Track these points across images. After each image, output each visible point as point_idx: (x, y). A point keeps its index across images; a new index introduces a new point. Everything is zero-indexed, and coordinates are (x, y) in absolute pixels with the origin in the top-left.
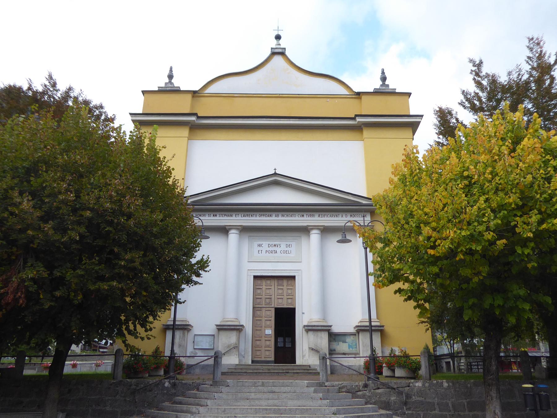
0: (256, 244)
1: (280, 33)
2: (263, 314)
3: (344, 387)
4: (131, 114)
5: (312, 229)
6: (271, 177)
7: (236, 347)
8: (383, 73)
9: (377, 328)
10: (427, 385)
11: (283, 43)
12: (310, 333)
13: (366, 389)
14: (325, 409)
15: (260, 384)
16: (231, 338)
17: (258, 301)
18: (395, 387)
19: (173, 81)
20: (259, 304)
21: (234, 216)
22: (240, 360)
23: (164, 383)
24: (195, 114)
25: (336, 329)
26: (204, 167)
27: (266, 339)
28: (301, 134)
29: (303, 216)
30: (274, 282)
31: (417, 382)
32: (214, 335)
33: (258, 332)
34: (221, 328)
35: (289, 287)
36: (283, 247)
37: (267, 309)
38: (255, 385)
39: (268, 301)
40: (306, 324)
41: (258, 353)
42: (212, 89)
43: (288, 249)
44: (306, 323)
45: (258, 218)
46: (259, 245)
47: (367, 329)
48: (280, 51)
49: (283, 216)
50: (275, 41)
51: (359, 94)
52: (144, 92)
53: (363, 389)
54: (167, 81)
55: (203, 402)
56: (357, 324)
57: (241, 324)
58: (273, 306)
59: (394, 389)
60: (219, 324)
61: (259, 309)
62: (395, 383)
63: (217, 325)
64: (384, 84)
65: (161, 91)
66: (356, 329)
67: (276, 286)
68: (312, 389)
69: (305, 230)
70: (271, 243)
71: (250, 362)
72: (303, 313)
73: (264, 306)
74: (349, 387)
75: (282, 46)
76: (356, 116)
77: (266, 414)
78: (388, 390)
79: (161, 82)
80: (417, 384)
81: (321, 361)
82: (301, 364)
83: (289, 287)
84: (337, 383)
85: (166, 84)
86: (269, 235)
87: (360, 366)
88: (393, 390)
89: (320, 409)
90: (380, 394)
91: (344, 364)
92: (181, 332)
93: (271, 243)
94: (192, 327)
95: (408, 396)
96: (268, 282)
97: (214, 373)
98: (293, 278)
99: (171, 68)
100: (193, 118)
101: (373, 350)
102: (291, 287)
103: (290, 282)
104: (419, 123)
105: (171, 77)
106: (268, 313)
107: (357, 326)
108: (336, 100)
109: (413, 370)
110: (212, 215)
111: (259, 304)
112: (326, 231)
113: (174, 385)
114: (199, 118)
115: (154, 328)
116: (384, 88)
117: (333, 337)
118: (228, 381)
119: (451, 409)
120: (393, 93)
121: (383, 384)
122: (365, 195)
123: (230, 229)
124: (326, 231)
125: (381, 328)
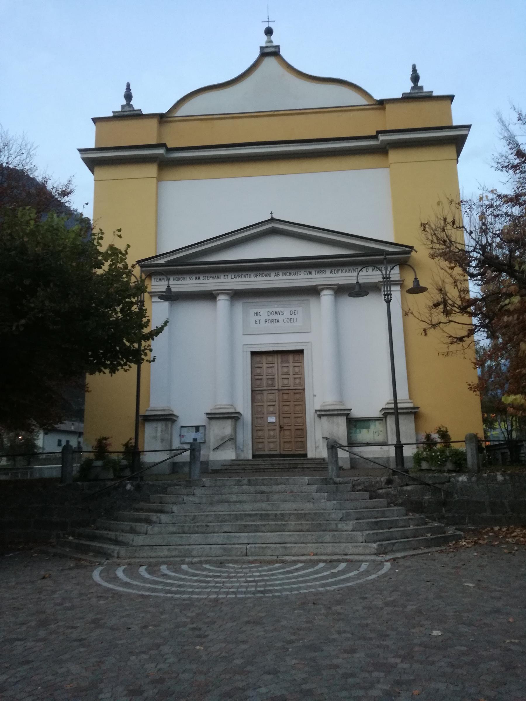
0: (252, 311)
1: (271, 25)
2: (265, 398)
3: (359, 484)
4: (80, 150)
5: (323, 289)
6: (268, 224)
7: (233, 439)
8: (414, 70)
9: (410, 411)
10: (474, 479)
11: (276, 39)
12: (324, 419)
13: (390, 486)
14: (329, 514)
15: (245, 482)
16: (225, 429)
17: (258, 382)
18: (431, 482)
20: (259, 386)
21: (222, 277)
22: (237, 455)
23: (126, 486)
24: (163, 145)
25: (357, 413)
27: (270, 428)
29: (310, 273)
30: (277, 359)
31: (460, 476)
32: (204, 426)
34: (212, 417)
36: (287, 314)
37: (270, 392)
38: (239, 483)
39: (270, 382)
40: (318, 408)
41: (260, 446)
42: (183, 111)
43: (293, 316)
45: (253, 279)
46: (257, 314)
47: (394, 412)
48: (272, 50)
49: (285, 274)
50: (265, 38)
52: (95, 120)
53: (387, 486)
54: (124, 102)
55: (167, 507)
56: (384, 407)
57: (238, 410)
58: (276, 388)
60: (209, 412)
62: (430, 478)
63: (207, 414)
65: (117, 117)
66: (383, 412)
67: (280, 364)
68: (314, 487)
69: (314, 291)
70: (270, 310)
71: (250, 457)
72: (315, 396)
73: (265, 388)
74: (367, 484)
75: (275, 44)
76: (379, 132)
77: (250, 521)
78: (420, 486)
79: (117, 104)
80: (460, 479)
81: (330, 450)
82: (314, 457)
84: (352, 478)
86: (269, 300)
87: (388, 458)
88: (428, 487)
89: (322, 514)
91: (366, 456)
92: (164, 423)
93: (270, 310)
94: (177, 417)
95: (448, 494)
96: (270, 359)
97: (190, 469)
98: (301, 352)
99: (128, 85)
100: (161, 151)
101: (172, 426)
103: (297, 357)
105: (128, 96)
106: (271, 397)
107: (383, 409)
109: (459, 462)
110: (194, 278)
111: (259, 386)
112: (340, 290)
113: (138, 488)
116: (416, 91)
117: (354, 423)
120: (429, 97)
121: (413, 479)
122: (393, 241)
123: (218, 294)
125: (416, 410)
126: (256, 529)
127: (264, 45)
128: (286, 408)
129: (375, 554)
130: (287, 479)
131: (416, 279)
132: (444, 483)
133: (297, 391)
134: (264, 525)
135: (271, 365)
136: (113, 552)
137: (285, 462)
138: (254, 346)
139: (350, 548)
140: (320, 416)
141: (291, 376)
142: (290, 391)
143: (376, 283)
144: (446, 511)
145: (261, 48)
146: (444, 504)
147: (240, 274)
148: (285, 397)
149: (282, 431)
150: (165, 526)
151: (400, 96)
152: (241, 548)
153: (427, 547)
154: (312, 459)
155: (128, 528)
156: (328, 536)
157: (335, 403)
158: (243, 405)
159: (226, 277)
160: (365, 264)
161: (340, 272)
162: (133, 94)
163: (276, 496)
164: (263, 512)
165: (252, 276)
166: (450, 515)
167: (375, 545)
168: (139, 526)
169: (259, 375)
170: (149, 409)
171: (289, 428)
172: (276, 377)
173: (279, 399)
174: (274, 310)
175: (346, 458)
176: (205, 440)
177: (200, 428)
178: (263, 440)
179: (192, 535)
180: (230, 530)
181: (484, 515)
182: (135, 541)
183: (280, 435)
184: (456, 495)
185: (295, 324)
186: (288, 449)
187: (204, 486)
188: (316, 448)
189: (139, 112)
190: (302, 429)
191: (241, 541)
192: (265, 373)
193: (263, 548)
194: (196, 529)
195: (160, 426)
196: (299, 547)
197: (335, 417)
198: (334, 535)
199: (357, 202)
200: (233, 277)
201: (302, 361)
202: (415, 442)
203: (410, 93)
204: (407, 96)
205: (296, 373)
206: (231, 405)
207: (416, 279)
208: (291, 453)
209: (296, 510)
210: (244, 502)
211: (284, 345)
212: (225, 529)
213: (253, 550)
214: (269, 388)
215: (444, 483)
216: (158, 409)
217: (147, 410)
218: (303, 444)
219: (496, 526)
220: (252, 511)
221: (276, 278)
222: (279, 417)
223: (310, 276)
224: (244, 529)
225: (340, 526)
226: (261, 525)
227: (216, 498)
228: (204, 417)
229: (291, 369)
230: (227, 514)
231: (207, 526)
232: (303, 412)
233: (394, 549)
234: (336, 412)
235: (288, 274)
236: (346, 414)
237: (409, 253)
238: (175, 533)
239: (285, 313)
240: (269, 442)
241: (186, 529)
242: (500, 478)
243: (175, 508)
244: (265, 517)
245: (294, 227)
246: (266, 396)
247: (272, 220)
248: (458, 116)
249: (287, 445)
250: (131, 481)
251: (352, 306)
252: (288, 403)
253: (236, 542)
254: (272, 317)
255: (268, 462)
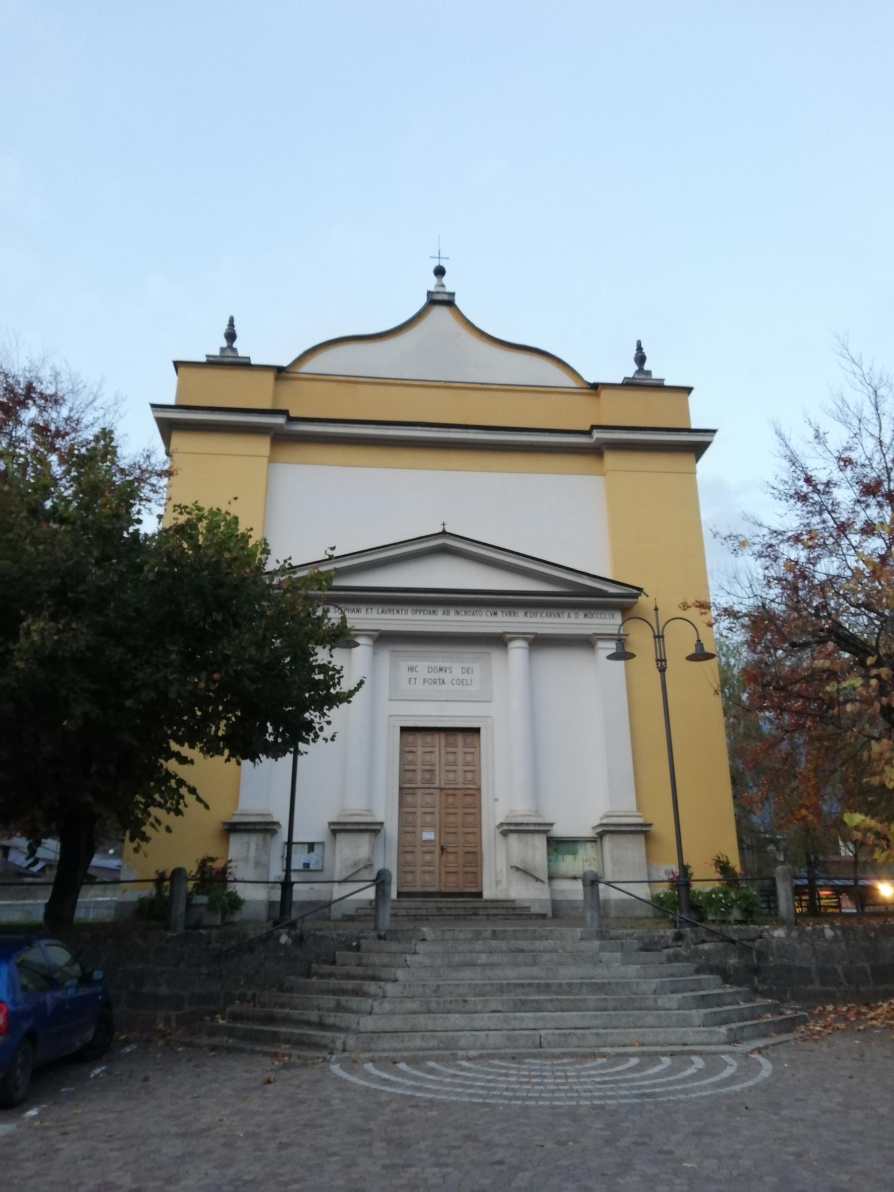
0: (404, 665)
1: (444, 263)
4: (153, 406)
5: (512, 639)
8: (639, 348)
9: (639, 828)
10: (794, 934)
11: (450, 283)
12: (513, 838)
13: (680, 943)
14: (638, 984)
15: (488, 934)
17: (409, 775)
18: (736, 938)
19: (235, 345)
20: (411, 781)
23: (279, 937)
24: (285, 413)
25: (560, 830)
26: (308, 516)
28: (456, 458)
29: (495, 614)
30: (439, 740)
31: (776, 929)
32: (322, 843)
33: (409, 838)
34: (338, 829)
35: (450, 750)
37: (427, 791)
39: (427, 776)
42: (313, 366)
44: (501, 819)
45: (410, 616)
46: (411, 669)
48: (445, 297)
49: (458, 613)
51: (595, 387)
52: (177, 365)
53: (675, 944)
54: (224, 343)
58: (437, 785)
59: (733, 942)
60: (334, 819)
61: (411, 791)
62: (735, 931)
64: (640, 370)
65: (212, 363)
69: (500, 641)
70: (433, 664)
72: (496, 800)
73: (419, 785)
74: (647, 940)
75: (449, 289)
76: (594, 427)
78: (721, 945)
79: (215, 345)
81: (589, 888)
83: (450, 750)
85: (222, 350)
88: (732, 945)
90: (707, 953)
93: (433, 664)
95: (762, 956)
96: (429, 739)
98: (477, 731)
99: (232, 321)
100: (281, 420)
102: (471, 750)
103: (470, 739)
104: (705, 446)
105: (231, 336)
106: (429, 799)
108: (554, 398)
111: (411, 781)
114: (291, 420)
115: (168, 829)
116: (642, 376)
117: (558, 845)
118: (424, 929)
119: (843, 979)
120: (659, 386)
121: (712, 933)
124: (539, 642)
126: (538, 1007)
127: (432, 289)
128: (451, 819)
129: (726, 1043)
130: (551, 931)
131: (699, 641)
132: (753, 940)
133: (468, 792)
134: (552, 1001)
135: (430, 749)
136: (333, 1041)
137: (458, 905)
138: (408, 718)
139: (675, 1034)
140: (505, 833)
141: (460, 768)
142: (458, 792)
143: (590, 635)
144: (759, 982)
145: (429, 293)
146: (756, 971)
147: (392, 608)
148: (451, 800)
149: (445, 854)
150: (401, 1002)
151: (619, 381)
152: (532, 1036)
153: (779, 1033)
154: (491, 901)
155: (332, 1004)
156: (650, 1018)
157: (528, 813)
158: (385, 810)
159: (369, 611)
160: (577, 605)
161: (539, 615)
162: (237, 333)
163: (546, 957)
164: (542, 982)
165: (410, 612)
166: (765, 987)
167: (723, 1029)
168: (354, 1002)
169: (412, 763)
170: (237, 812)
171: (456, 850)
172: (437, 768)
173: (440, 801)
174: (439, 664)
175: (546, 900)
176: (323, 866)
177: (316, 847)
178: (414, 869)
179: (450, 1016)
180: (500, 1008)
181: (810, 987)
182: (361, 1025)
183: (440, 862)
184: (771, 959)
185: (467, 688)
186: (452, 884)
187: (424, 940)
188: (498, 883)
189: (247, 361)
190: (475, 853)
191: (524, 1025)
192: (419, 762)
193: (565, 1035)
194: (448, 1006)
195: (254, 840)
196: (618, 1034)
197: (530, 835)
198: (660, 1016)
199: (561, 518)
200: (380, 611)
201: (478, 746)
202: (646, 879)
203: (633, 378)
204: (628, 381)
205: (467, 764)
206: (369, 811)
207: (699, 641)
208: (456, 890)
209: (582, 978)
210: (498, 965)
211: (453, 719)
212: (493, 1007)
213: (551, 1038)
214: (465, 786)
215: (753, 940)
216: (253, 812)
217: (234, 815)
218: (477, 876)
219: (828, 1004)
220: (517, 979)
221: (445, 617)
222: (440, 832)
223: (494, 619)
224: (521, 1006)
225: (660, 1002)
226: (547, 1000)
227: (456, 959)
228: (325, 827)
229: (460, 756)
230: (488, 984)
231: (465, 1001)
232: (478, 825)
233: (744, 1036)
234: (532, 828)
235: (463, 613)
236: (542, 829)
237: (636, 596)
238: (415, 1013)
239: (454, 670)
240: (424, 872)
241: (433, 1006)
242: (829, 933)
243: (400, 974)
244: (546, 988)
245: (460, 542)
246: (420, 798)
247: (444, 533)
248: (699, 416)
249: (452, 878)
250: (286, 930)
251: (558, 665)
252: (453, 811)
253: (518, 1027)
254: (434, 676)
255: (431, 905)
